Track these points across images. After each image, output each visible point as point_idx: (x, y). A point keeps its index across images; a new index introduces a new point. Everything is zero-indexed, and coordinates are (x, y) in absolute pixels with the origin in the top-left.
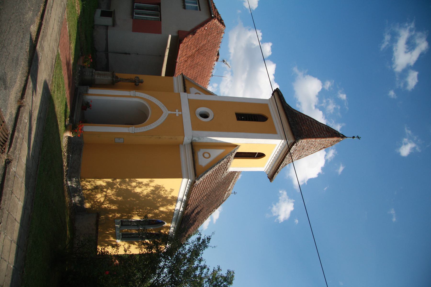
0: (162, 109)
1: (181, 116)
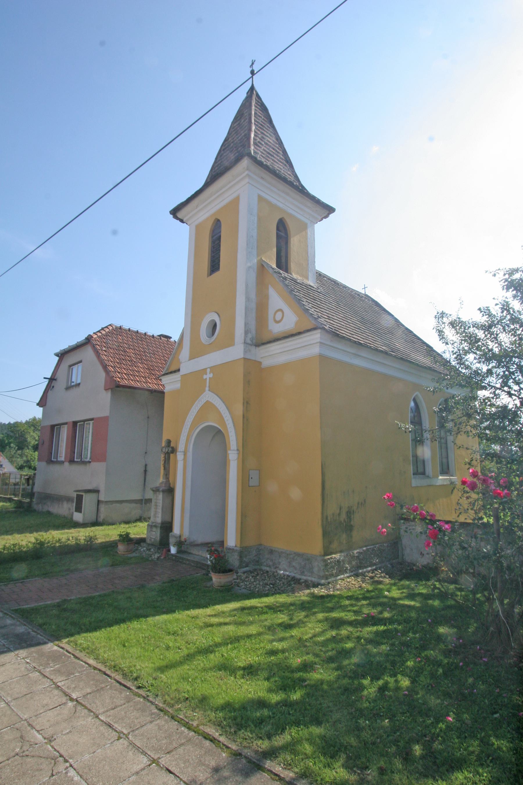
0: (203, 403)
1: (212, 368)
